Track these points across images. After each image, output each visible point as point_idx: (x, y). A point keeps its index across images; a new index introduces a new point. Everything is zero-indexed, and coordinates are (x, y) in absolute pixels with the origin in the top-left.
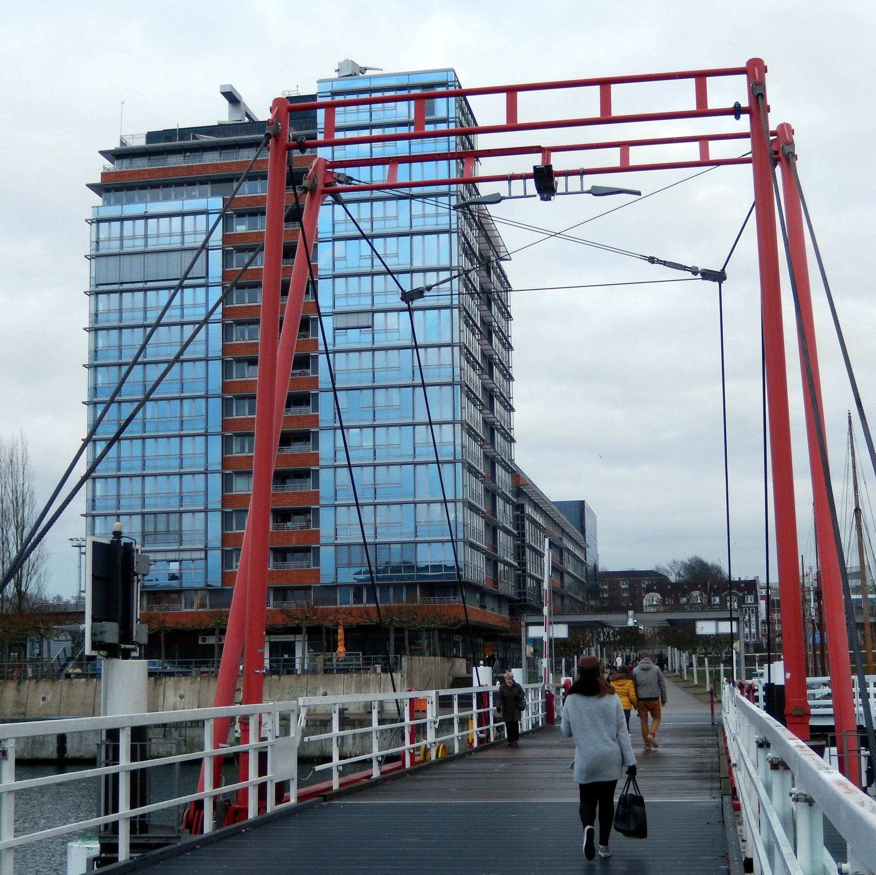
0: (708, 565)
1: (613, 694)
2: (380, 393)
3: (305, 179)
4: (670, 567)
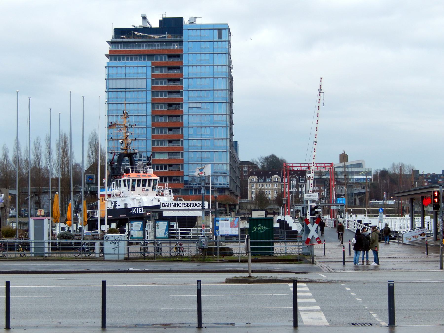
0: (279, 159)
1: (279, 215)
2: (203, 129)
3: (306, 193)
4: (259, 160)
